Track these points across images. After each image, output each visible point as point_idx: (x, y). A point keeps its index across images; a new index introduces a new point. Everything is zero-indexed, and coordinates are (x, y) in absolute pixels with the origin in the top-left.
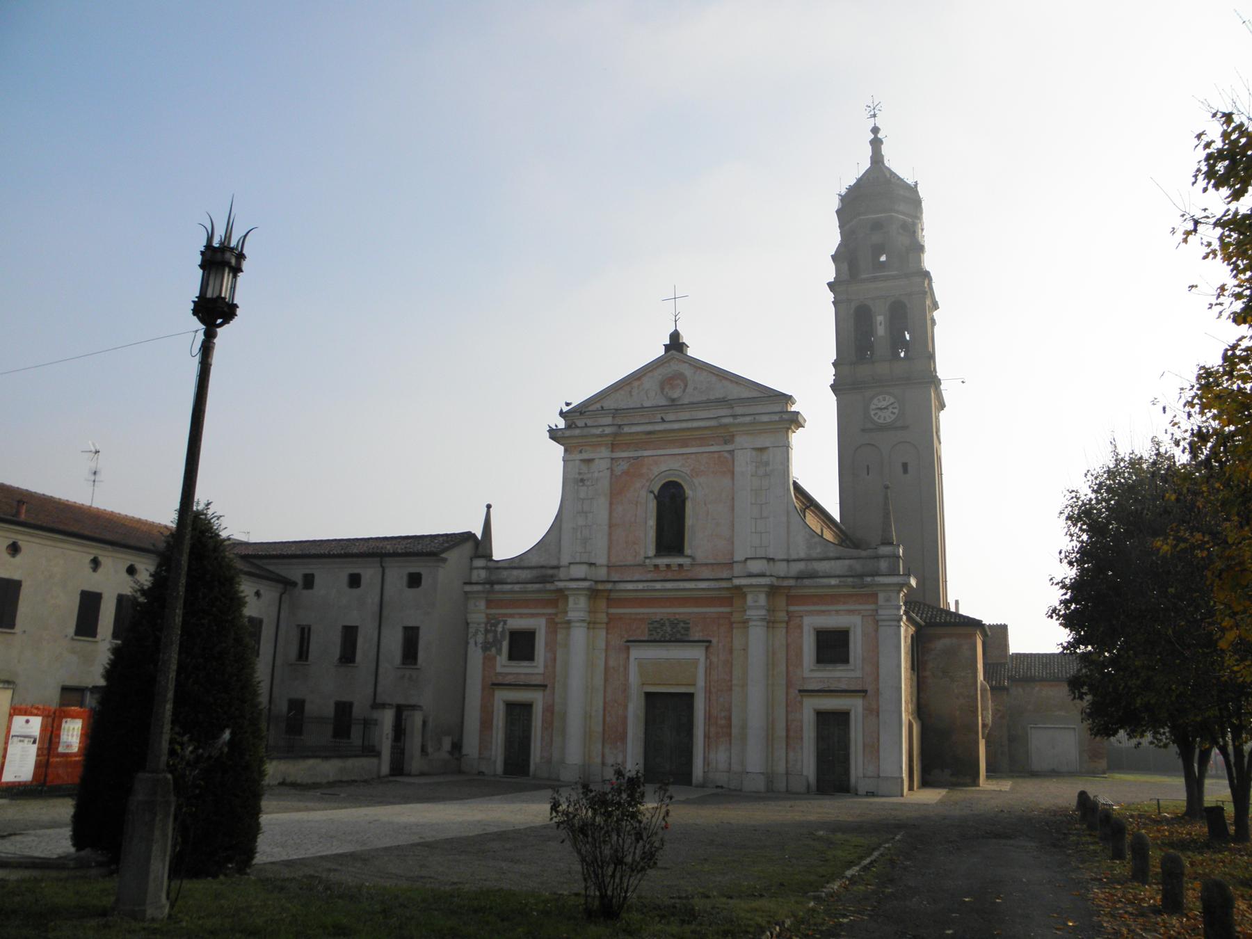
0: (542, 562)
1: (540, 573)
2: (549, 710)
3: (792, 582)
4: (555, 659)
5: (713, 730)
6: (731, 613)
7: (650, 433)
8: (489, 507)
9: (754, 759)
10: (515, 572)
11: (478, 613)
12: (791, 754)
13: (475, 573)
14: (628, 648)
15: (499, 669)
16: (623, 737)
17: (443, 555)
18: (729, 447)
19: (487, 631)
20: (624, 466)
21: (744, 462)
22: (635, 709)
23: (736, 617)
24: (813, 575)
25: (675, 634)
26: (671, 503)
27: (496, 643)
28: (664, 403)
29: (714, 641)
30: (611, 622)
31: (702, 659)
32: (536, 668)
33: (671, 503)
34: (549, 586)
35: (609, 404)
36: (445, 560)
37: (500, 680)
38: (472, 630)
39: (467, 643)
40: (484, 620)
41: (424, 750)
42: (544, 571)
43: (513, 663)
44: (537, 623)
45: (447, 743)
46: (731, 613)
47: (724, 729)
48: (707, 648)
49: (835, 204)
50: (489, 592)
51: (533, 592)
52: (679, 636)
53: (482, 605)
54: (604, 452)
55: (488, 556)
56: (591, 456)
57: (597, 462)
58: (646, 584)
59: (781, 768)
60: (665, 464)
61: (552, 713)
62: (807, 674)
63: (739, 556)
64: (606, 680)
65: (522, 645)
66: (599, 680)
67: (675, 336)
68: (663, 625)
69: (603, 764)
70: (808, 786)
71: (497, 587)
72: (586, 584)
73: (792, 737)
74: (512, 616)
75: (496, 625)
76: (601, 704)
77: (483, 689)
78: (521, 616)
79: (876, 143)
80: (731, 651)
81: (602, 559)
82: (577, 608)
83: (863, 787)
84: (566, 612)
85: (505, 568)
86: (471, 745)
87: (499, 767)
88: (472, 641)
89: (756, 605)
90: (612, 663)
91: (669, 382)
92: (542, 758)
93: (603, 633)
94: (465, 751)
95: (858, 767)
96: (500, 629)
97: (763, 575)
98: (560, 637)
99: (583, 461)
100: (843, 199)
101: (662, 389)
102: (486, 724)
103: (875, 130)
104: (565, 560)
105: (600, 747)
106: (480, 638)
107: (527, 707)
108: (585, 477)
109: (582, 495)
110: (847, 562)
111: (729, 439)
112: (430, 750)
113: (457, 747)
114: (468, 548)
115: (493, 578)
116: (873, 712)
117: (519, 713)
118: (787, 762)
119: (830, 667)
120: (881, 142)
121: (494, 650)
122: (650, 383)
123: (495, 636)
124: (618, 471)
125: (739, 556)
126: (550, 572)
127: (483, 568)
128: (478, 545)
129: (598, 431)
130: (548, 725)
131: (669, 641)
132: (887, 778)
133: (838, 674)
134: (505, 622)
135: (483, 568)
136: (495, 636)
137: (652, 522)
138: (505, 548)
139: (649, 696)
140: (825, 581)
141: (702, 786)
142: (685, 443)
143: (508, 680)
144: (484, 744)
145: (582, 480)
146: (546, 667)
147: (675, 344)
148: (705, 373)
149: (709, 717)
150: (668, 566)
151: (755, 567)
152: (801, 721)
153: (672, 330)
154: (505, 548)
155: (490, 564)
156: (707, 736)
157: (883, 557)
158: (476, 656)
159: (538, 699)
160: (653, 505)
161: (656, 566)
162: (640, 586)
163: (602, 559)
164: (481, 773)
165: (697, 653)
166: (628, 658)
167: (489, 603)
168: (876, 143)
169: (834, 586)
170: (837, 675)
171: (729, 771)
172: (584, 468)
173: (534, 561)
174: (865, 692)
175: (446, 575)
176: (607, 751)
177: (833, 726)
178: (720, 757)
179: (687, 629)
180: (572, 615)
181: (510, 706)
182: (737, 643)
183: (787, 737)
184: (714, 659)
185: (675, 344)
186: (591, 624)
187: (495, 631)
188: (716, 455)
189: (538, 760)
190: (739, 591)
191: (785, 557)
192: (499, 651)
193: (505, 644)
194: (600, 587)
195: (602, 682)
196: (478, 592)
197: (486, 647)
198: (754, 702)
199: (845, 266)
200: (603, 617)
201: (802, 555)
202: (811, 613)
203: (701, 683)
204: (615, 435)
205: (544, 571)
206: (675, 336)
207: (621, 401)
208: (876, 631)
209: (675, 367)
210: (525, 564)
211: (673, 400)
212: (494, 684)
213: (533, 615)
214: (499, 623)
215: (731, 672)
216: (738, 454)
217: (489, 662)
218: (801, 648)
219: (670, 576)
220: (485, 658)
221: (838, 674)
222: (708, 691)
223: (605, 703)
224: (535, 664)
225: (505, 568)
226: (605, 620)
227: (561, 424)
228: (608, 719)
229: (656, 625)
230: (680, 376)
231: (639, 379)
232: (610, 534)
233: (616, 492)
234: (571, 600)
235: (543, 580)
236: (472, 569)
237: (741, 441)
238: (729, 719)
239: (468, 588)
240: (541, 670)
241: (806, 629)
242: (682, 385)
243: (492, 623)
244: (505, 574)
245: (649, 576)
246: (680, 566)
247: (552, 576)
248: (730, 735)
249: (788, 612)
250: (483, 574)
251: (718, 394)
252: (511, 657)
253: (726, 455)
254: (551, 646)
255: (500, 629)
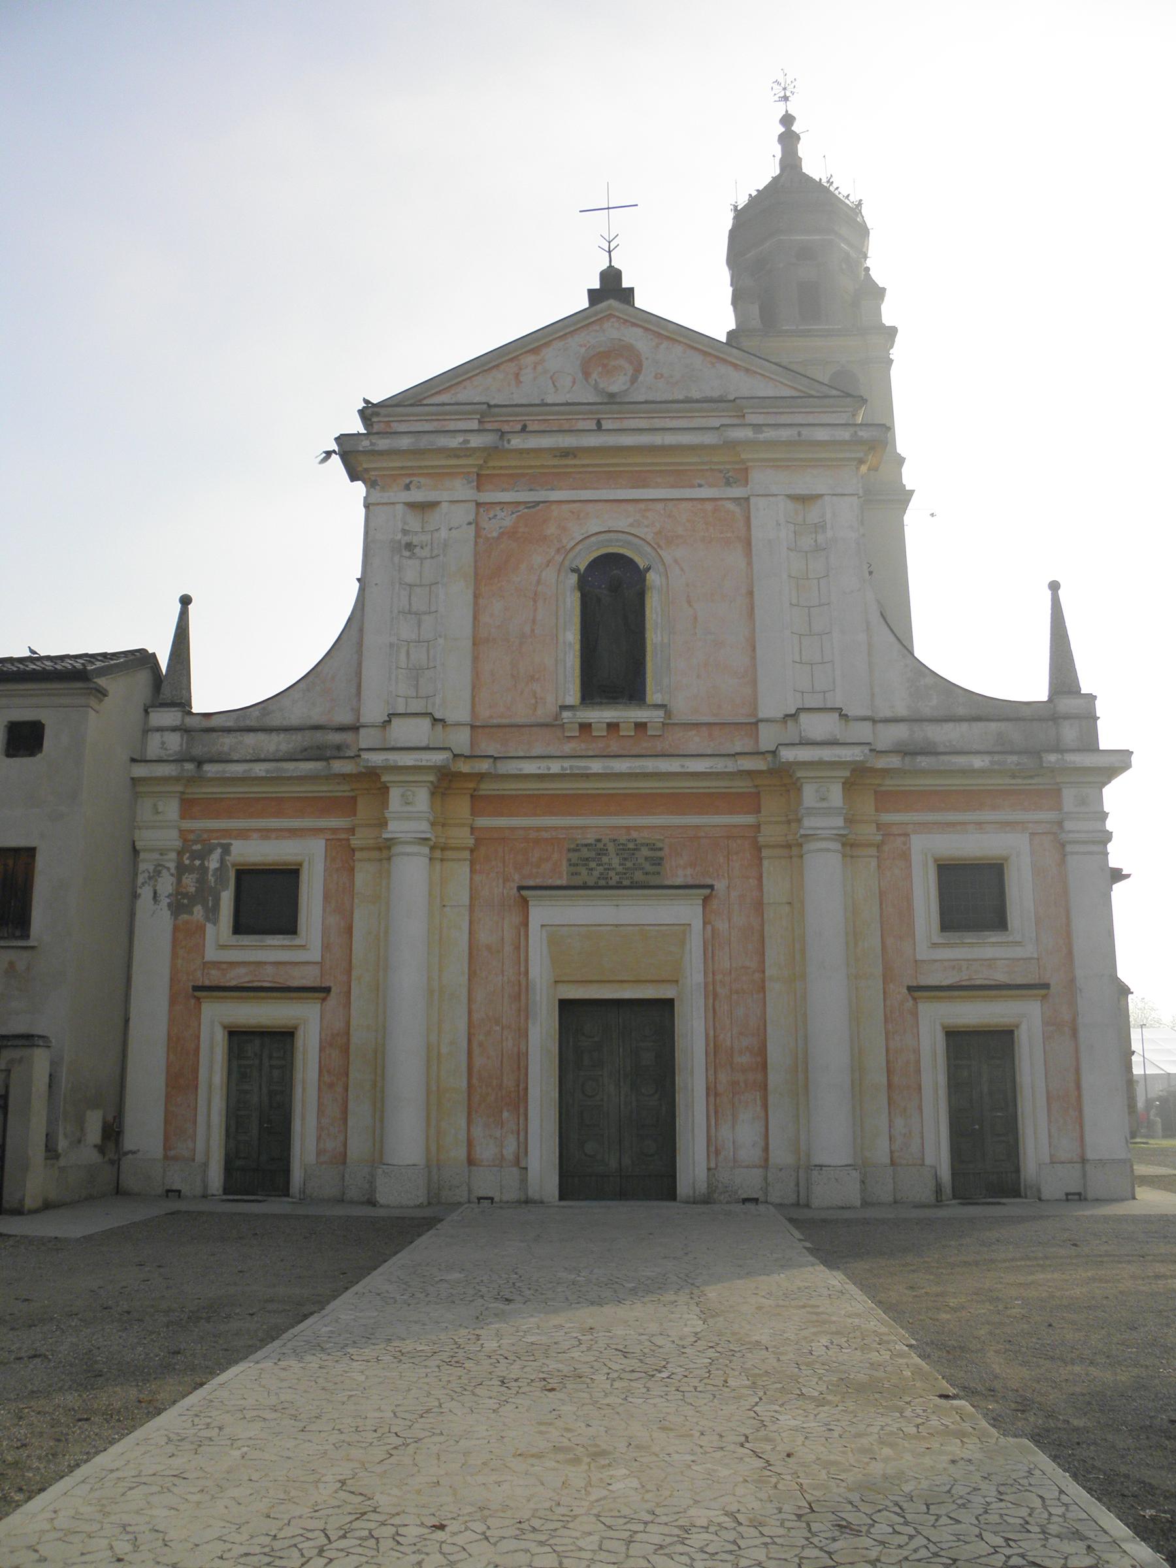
0: (317, 716)
1: (315, 746)
2: (338, 1043)
3: (894, 762)
4: (349, 930)
5: (723, 1077)
6: (758, 827)
7: (566, 453)
8: (186, 601)
9: (832, 1137)
10: (250, 739)
11: (163, 828)
12: (899, 1122)
13: (154, 740)
14: (525, 902)
15: (211, 954)
16: (518, 1100)
17: (101, 682)
18: (737, 492)
19: (181, 870)
20: (507, 520)
21: (770, 520)
22: (543, 1033)
23: (771, 833)
24: (929, 750)
25: (627, 870)
26: (613, 602)
27: (205, 896)
28: (592, 399)
29: (720, 886)
30: (481, 847)
31: (697, 924)
32: (307, 948)
33: (613, 602)
34: (338, 766)
35: (469, 393)
36: (102, 693)
37: (215, 977)
38: (146, 865)
39: (135, 896)
40: (178, 844)
41: (51, 1152)
42: (319, 737)
43: (246, 940)
44: (309, 853)
45: (94, 1133)
46: (758, 827)
47: (746, 1073)
48: (706, 900)
49: (727, 222)
50: (191, 780)
51: (302, 779)
52: (639, 876)
53: (171, 809)
54: (462, 490)
55: (183, 703)
56: (432, 496)
57: (444, 505)
58: (567, 764)
59: (881, 1152)
60: (598, 519)
61: (346, 1050)
62: (923, 953)
63: (770, 707)
64: (472, 975)
65: (267, 901)
66: (456, 972)
67: (611, 277)
68: (603, 852)
69: (471, 1162)
70: (939, 1190)
71: (211, 769)
72: (438, 758)
73: (899, 1086)
74: (243, 834)
75: (203, 855)
76: (462, 1025)
77: (173, 1001)
78: (266, 834)
79: (789, 140)
80: (759, 906)
81: (459, 712)
82: (409, 812)
83: (1054, 1184)
84: (383, 824)
85: (228, 730)
86: (145, 1131)
87: (216, 1177)
88: (146, 893)
89: (824, 805)
90: (484, 937)
91: (598, 361)
92: (319, 1153)
93: (465, 869)
94: (129, 1143)
95: (1039, 1145)
96: (213, 863)
97: (833, 743)
98: (364, 876)
99: (412, 506)
100: (741, 216)
101: (586, 375)
102: (181, 1081)
103: (787, 120)
104: (373, 712)
105: (463, 1123)
106: (166, 885)
107: (282, 1039)
108: (415, 540)
109: (410, 576)
110: (993, 726)
111: (741, 475)
112: (62, 1144)
113: (113, 1133)
114: (123, 693)
115: (198, 751)
116: (1065, 1027)
117: (261, 1056)
118: (891, 1138)
119: (970, 938)
120: (797, 138)
121: (198, 911)
122: (561, 362)
123: (202, 881)
124: (492, 528)
125: (770, 707)
126: (336, 738)
127: (174, 729)
128: (159, 681)
129: (454, 442)
130: (336, 1077)
131: (619, 887)
132: (1102, 1162)
133: (989, 952)
134: (226, 849)
135: (174, 729)
136: (202, 881)
137: (572, 636)
138: (215, 690)
139: (566, 1007)
140: (961, 761)
141: (706, 1200)
142: (640, 479)
143: (234, 977)
144: (176, 1125)
145: (409, 546)
146: (326, 947)
147: (611, 289)
148: (678, 349)
149: (714, 1050)
150: (613, 727)
151: (817, 726)
152: (917, 1052)
153: (605, 265)
154: (215, 690)
155: (189, 721)
156: (712, 1091)
157: (1067, 717)
158: (155, 926)
159: (308, 1021)
160: (572, 602)
161: (585, 727)
162: (555, 767)
163: (459, 712)
164: (173, 1193)
165: (684, 912)
166: (526, 924)
167: (188, 806)
168: (789, 140)
169: (982, 772)
170: (982, 954)
171: (765, 1164)
172: (414, 523)
173: (296, 714)
174: (1046, 986)
175: (96, 733)
176: (477, 1132)
177: (980, 1059)
178: (743, 1135)
179: (658, 862)
180: (395, 828)
181: (238, 1036)
182: (775, 886)
183: (890, 1085)
184: (722, 926)
185: (611, 289)
186: (438, 850)
187: (203, 870)
188: (709, 506)
189: (311, 1158)
190: (783, 778)
191: (869, 713)
192: (212, 913)
193: (227, 898)
194: (464, 767)
195: (464, 980)
196: (165, 780)
197: (179, 906)
198: (829, 1011)
199: (755, 310)
200: (462, 836)
201: (901, 710)
202: (925, 827)
203: (695, 975)
204: (490, 452)
205: (319, 737)
206: (611, 277)
207: (496, 390)
208: (1063, 861)
209: (612, 332)
210: (275, 720)
211: (612, 395)
212: (197, 988)
213: (293, 833)
214: (211, 851)
215: (762, 954)
216: (759, 506)
217: (186, 938)
218: (909, 899)
219: (614, 747)
220: (176, 929)
221: (989, 952)
222: (711, 994)
223: (470, 1025)
224: (298, 941)
225: (228, 730)
226: (471, 842)
227: (358, 427)
228: (478, 1062)
229: (585, 853)
230: (626, 351)
231: (535, 351)
232: (475, 659)
233: (489, 572)
234: (395, 794)
235: (318, 753)
236: (146, 731)
237: (761, 479)
238: (762, 1051)
239: (140, 771)
240: (314, 954)
241: (916, 858)
242: (630, 372)
243: (192, 853)
244: (226, 742)
245: (568, 748)
246: (641, 726)
247: (339, 748)
248: (764, 1087)
249: (879, 827)
250: (174, 742)
251: (711, 388)
252: (239, 928)
253: (731, 506)
254: (341, 901)
255: (213, 863)
